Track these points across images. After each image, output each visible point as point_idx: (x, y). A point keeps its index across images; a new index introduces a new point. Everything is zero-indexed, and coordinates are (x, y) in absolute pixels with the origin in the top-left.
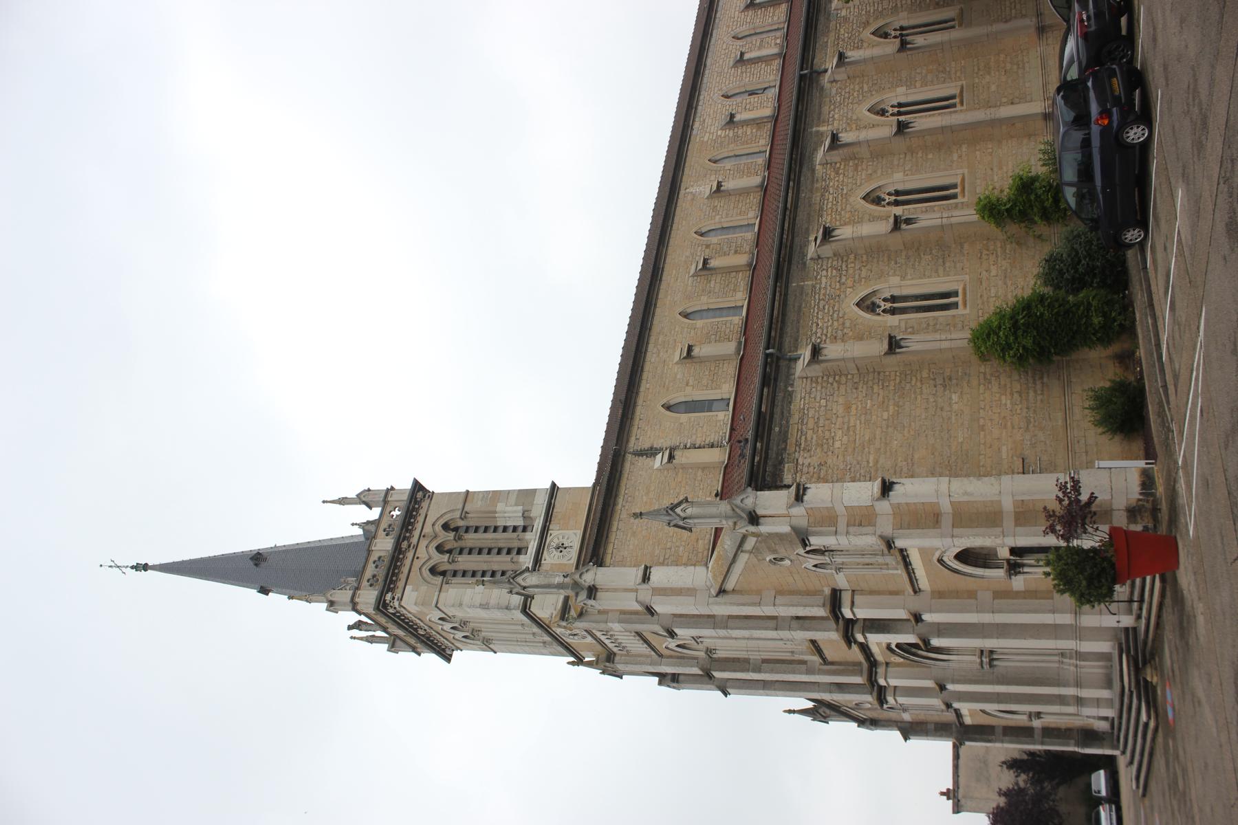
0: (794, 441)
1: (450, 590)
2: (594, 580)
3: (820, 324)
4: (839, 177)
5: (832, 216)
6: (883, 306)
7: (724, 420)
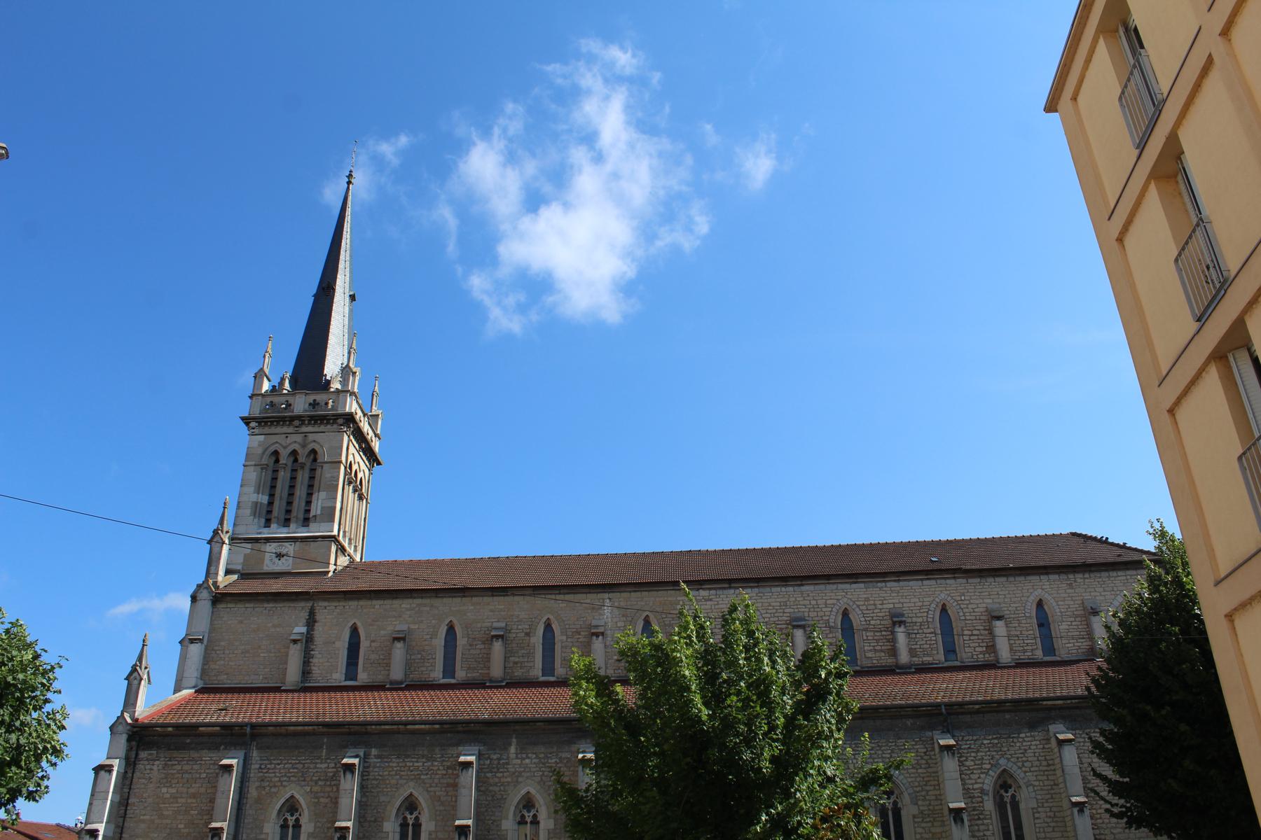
1: (255, 473)
3: (278, 767)
4: (444, 769)
5: (396, 767)
6: (411, 817)
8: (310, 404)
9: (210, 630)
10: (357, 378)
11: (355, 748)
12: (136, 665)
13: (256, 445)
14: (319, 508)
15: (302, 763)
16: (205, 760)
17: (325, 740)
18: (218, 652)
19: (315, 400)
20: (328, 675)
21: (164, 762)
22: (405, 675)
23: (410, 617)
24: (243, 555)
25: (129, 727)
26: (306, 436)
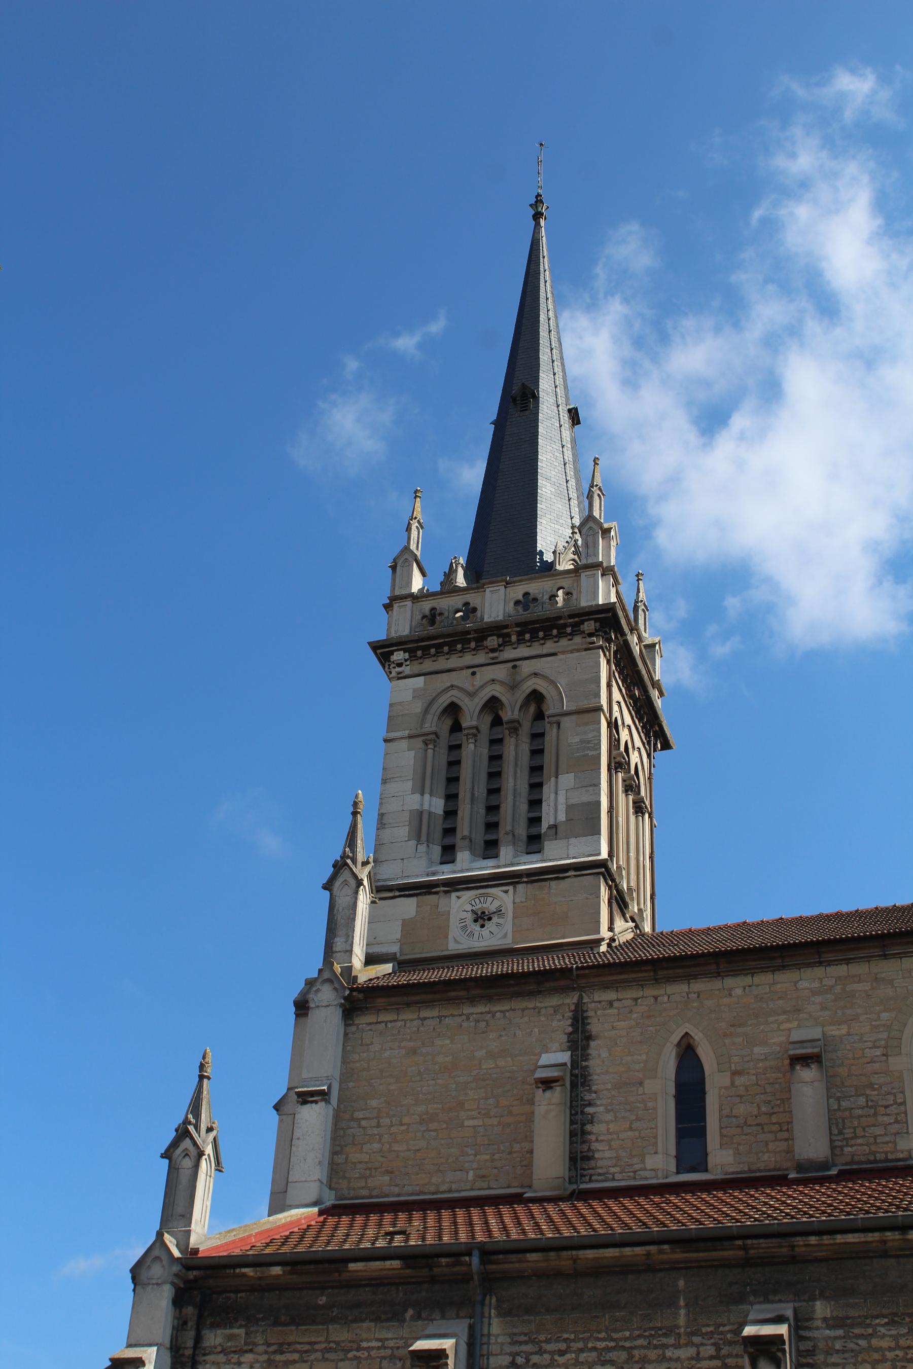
0: (290, 1339)
1: (412, 753)
2: (318, 1007)
3: (561, 1360)
5: (890, 1349)
7: (645, 1169)
8: (517, 603)
9: (342, 1074)
10: (613, 543)
11: (767, 1301)
12: (186, 1122)
13: (408, 696)
14: (562, 808)
15: (623, 1348)
16: (368, 1349)
17: (681, 1283)
18: (363, 1123)
19: (526, 594)
20: (635, 1160)
21: (265, 1357)
22: (833, 1148)
23: (822, 1010)
24: (400, 922)
25: (176, 1268)
26: (514, 667)
